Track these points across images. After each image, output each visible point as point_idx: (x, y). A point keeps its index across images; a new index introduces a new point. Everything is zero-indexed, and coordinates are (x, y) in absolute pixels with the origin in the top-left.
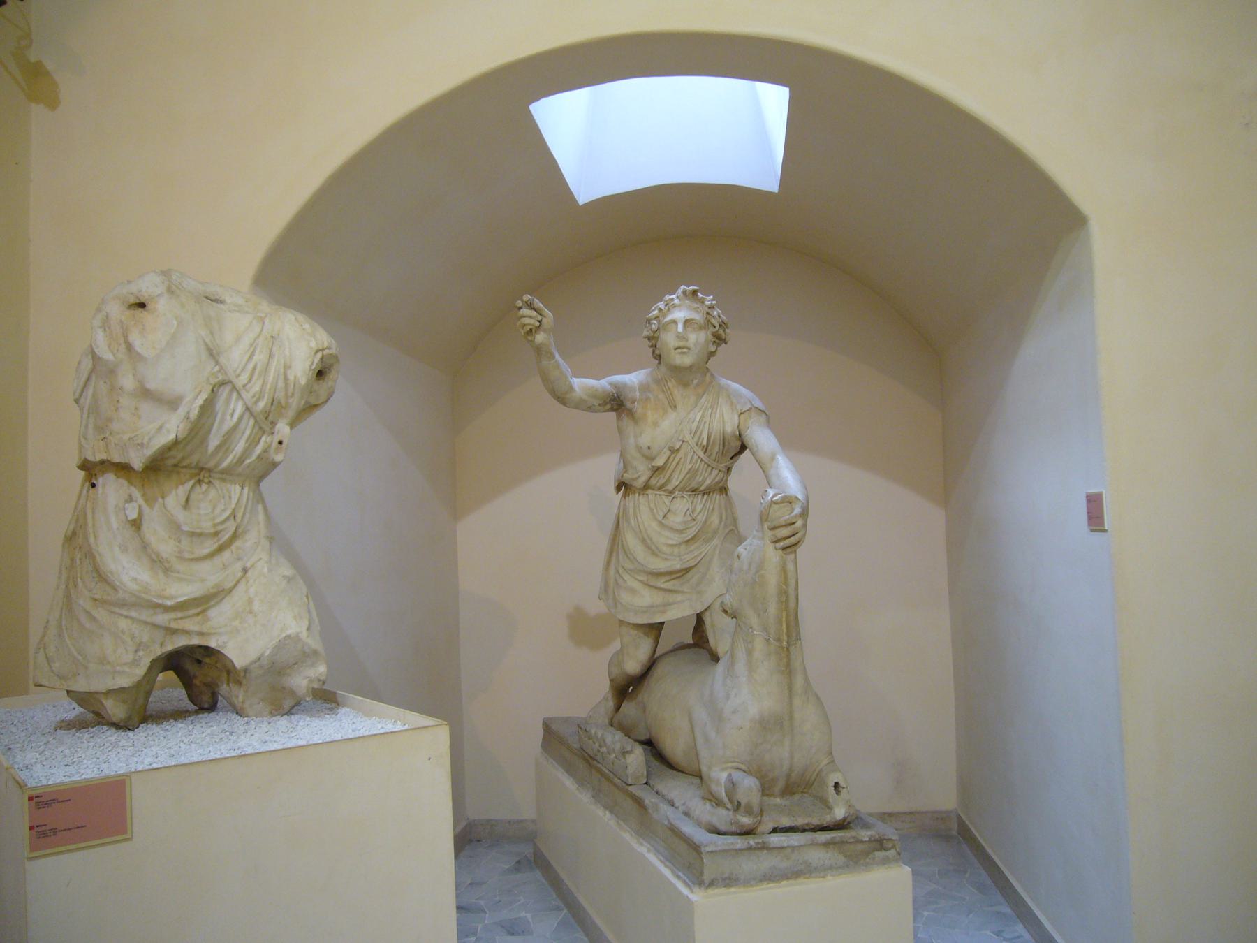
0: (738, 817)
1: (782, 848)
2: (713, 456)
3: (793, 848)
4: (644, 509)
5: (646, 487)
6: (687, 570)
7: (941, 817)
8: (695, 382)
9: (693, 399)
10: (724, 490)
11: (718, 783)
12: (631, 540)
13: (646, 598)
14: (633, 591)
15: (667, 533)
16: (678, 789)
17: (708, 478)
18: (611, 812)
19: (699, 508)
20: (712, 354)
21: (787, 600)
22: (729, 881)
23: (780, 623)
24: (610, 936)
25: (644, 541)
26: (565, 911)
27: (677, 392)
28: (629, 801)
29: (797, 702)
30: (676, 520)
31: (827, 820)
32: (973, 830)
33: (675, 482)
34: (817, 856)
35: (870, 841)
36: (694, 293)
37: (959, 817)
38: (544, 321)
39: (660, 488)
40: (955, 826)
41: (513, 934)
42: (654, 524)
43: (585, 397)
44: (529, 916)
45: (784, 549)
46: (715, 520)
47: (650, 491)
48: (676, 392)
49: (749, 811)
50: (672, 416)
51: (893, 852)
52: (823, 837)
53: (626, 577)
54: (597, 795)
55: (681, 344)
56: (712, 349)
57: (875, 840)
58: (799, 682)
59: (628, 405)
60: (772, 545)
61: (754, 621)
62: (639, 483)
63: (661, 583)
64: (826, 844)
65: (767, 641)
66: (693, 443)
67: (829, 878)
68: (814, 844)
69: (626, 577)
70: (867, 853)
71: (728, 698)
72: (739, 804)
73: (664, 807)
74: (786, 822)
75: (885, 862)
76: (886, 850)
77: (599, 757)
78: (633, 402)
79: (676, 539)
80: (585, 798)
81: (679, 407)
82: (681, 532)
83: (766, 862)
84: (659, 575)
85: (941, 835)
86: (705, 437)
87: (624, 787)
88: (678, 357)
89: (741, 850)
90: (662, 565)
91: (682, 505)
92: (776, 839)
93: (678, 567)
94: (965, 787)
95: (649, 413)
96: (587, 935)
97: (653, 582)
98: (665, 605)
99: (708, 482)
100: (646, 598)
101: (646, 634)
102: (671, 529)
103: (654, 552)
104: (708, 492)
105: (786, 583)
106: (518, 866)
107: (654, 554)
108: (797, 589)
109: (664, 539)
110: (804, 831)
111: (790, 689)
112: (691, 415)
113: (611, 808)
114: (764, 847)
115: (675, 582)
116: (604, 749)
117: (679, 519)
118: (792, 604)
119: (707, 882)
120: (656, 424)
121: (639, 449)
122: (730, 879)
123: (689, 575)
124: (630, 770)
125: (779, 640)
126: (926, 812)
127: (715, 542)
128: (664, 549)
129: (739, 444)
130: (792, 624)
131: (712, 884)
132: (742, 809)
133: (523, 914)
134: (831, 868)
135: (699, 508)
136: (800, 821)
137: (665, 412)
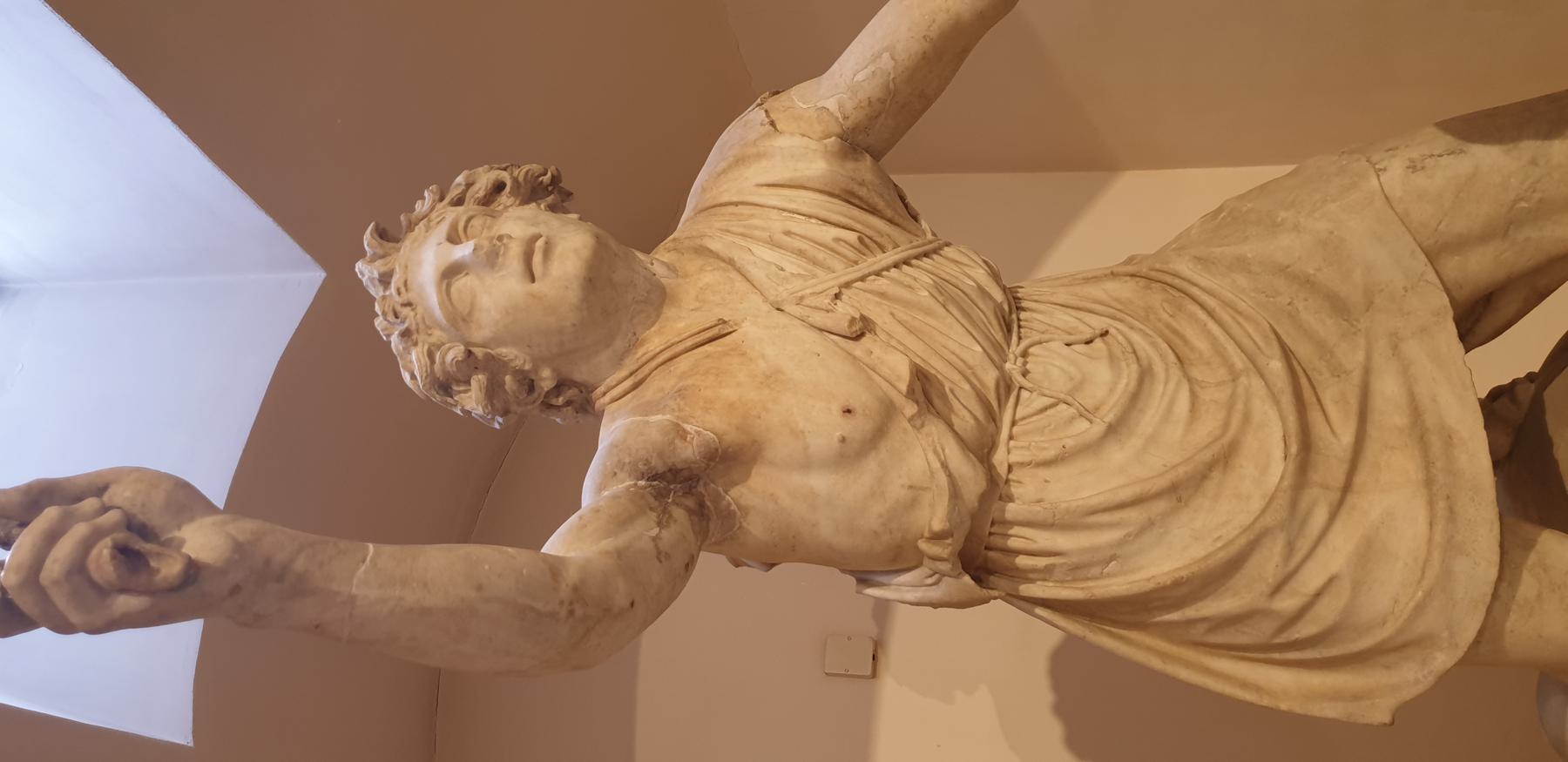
5: (982, 450)
12: (1159, 563)
13: (1393, 503)
14: (1368, 553)
15: (1147, 421)
27: (680, 322)
33: (974, 352)
42: (1117, 455)
43: (608, 544)
47: (1000, 458)
59: (688, 452)
63: (1337, 435)
69: (1311, 579)
78: (683, 434)
79: (1168, 392)
82: (1145, 374)
90: (1266, 460)
91: (1050, 365)
95: (728, 393)
97: (1330, 469)
100: (1393, 503)
101: (1528, 545)
102: (1136, 398)
107: (1224, 458)
109: (1169, 435)
110: (1495, 595)
112: (757, 273)
115: (1328, 397)
117: (1101, 373)
120: (772, 379)
121: (850, 454)
128: (1209, 425)
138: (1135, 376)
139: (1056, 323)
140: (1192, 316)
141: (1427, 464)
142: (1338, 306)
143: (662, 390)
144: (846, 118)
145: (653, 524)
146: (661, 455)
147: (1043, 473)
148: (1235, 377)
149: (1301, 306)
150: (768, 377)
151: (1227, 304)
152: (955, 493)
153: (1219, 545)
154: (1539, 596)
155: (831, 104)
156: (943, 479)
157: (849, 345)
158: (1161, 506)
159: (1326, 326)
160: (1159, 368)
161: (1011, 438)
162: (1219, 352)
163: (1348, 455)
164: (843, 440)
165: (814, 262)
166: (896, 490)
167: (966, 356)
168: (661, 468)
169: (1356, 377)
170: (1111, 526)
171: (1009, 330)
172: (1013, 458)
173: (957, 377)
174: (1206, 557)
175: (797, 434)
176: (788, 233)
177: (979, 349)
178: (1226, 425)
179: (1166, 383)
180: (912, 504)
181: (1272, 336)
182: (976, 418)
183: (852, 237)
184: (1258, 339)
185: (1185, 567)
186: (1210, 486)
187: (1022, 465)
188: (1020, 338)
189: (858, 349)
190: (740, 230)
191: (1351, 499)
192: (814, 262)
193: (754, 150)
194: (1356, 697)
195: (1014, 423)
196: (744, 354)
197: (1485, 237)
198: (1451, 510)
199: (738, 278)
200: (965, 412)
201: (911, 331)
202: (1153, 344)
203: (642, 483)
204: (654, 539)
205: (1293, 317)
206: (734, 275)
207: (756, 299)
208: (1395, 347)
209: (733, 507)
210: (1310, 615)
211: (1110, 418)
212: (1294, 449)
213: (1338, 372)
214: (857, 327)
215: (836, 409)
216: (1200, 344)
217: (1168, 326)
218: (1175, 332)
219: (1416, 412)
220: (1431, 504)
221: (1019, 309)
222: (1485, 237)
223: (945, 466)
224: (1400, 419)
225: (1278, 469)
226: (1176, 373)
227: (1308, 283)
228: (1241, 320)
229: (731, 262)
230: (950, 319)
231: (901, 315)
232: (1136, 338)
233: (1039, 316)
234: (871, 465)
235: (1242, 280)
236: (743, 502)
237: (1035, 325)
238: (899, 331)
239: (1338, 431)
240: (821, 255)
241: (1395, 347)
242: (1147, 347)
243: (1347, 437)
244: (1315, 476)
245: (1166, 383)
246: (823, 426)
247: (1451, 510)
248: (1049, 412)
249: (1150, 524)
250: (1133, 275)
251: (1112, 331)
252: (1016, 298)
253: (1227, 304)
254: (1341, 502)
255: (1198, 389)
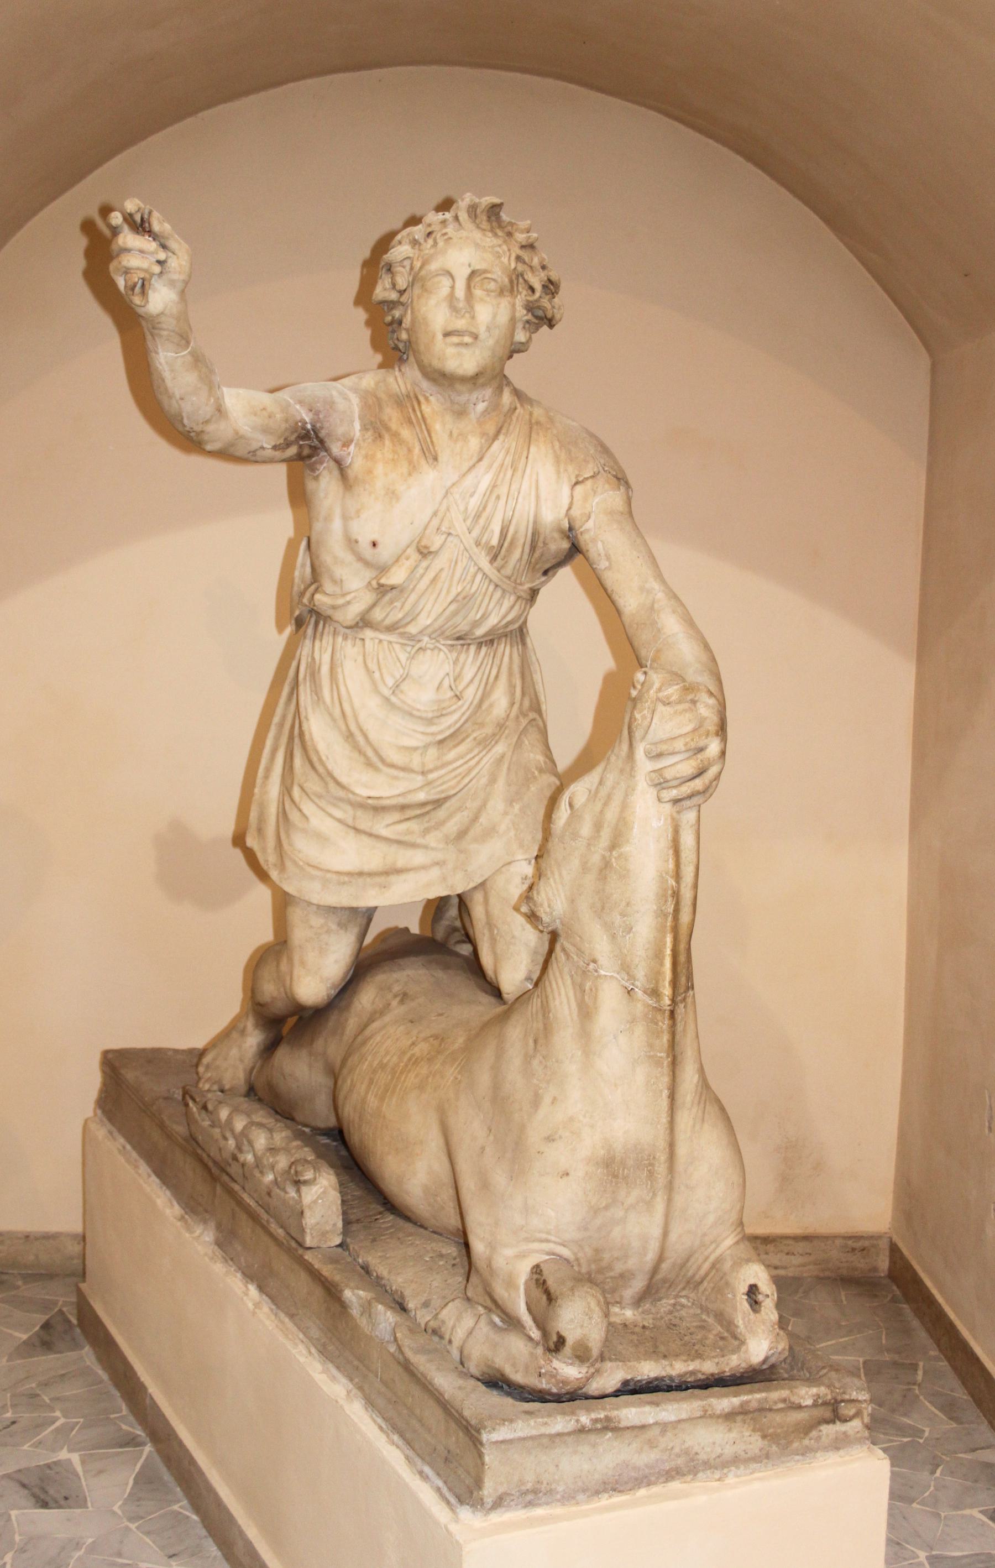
0: (556, 1364)
1: (643, 1427)
2: (508, 571)
3: (664, 1427)
4: (353, 676)
5: (364, 622)
6: (438, 803)
7: (859, 1244)
8: (481, 406)
9: (474, 443)
10: (517, 634)
11: (510, 1283)
12: (319, 729)
13: (348, 853)
14: (321, 838)
16: (407, 1266)
17: (497, 612)
18: (261, 1288)
19: (468, 674)
20: (515, 350)
21: (677, 911)
22: (534, 1495)
23: (659, 956)
24: (265, 1552)
25: (349, 736)
26: (148, 1448)
28: (303, 1276)
29: (685, 1119)
30: (422, 696)
31: (733, 1363)
32: (929, 1283)
33: (424, 620)
34: (711, 1439)
35: (815, 1405)
36: (494, 211)
37: (894, 1249)
38: (173, 263)
39: (391, 628)
40: (883, 1264)
41: (45, 1505)
42: (373, 703)
44: (75, 1458)
45: (676, 801)
46: (500, 702)
47: (368, 633)
48: (437, 427)
49: (582, 1355)
50: (429, 477)
51: (856, 1424)
52: (725, 1402)
53: (308, 808)
54: (226, 1242)
55: (460, 324)
56: (521, 336)
57: (825, 1404)
58: (689, 1077)
59: (336, 449)
60: (653, 792)
61: (601, 946)
62: (352, 613)
63: (383, 826)
64: (729, 1416)
65: (629, 992)
66: (469, 540)
67: (731, 1480)
68: (707, 1416)
70: (807, 1428)
71: (536, 1102)
72: (561, 1341)
73: (386, 1318)
74: (648, 1370)
75: (839, 1444)
76: (845, 1420)
77: (234, 1169)
78: (346, 444)
80: (200, 1240)
81: (443, 457)
83: (610, 1455)
84: (378, 809)
85: (856, 1282)
86: (496, 528)
87: (294, 1246)
88: (451, 351)
89: (559, 1435)
90: (366, 784)
92: (633, 1412)
93: (421, 796)
94: (910, 1197)
95: (379, 469)
96: (197, 1509)
97: (365, 821)
98: (386, 873)
99: (493, 621)
100: (348, 853)
101: (342, 926)
103: (372, 759)
104: (490, 640)
105: (678, 876)
106: (48, 1338)
108: (695, 886)
109: (393, 734)
111: (672, 1097)
112: (469, 480)
113: (259, 1277)
114: (609, 1426)
115: (413, 825)
116: (250, 1158)
118: (685, 918)
119: (489, 1501)
120: (392, 495)
122: (535, 1492)
123: (441, 813)
124: (310, 1220)
125: (655, 993)
126: (835, 1237)
127: (500, 749)
129: (565, 545)
130: (682, 958)
131: (499, 1503)
132: (567, 1350)
133: (63, 1455)
134: (736, 1461)
135: (468, 674)
136: (678, 1368)
137: (413, 468)
138: (424, 715)
139: (466, 668)
140: (471, 750)
141: (371, 874)
142: (462, 834)
143: (390, 419)
144: (581, 533)
145: (273, 444)
146: (329, 435)
147: (360, 659)
148: (423, 773)
149: (465, 813)
150: (393, 493)
151: (470, 770)
152: (334, 607)
153: (324, 758)
154: (311, 927)
155: (590, 524)
156: (341, 601)
157: (414, 544)
158: (344, 728)
159: (452, 827)
160: (434, 729)
161: (381, 641)
162: (443, 766)
163: (374, 831)
164: (357, 542)
165: (478, 516)
166: (339, 572)
167: (423, 615)
168: (322, 434)
169: (420, 841)
170: (332, 698)
171: (458, 638)
172: (367, 642)
173: (407, 607)
174: (317, 752)
175: (358, 512)
176: (498, 497)
177: (429, 622)
178: (392, 766)
179: (422, 733)
180: (334, 582)
181: (443, 795)
182: (383, 620)
183: (495, 542)
184: (444, 787)
185: (312, 739)
186: (356, 755)
187: (364, 645)
188: (452, 646)
189: (411, 551)
190: (506, 463)
191: (352, 833)
192: (478, 516)
193: (562, 470)
194: (260, 831)
195: (390, 642)
196: (410, 474)
197: (487, 913)
198: (344, 883)
199: (471, 463)
200: (384, 615)
201: (434, 581)
202: (449, 727)
203: (309, 426)
204: (262, 448)
205: (459, 809)
206: (475, 459)
207: (455, 478)
208: (437, 864)
209: (317, 473)
210: (293, 806)
211: (393, 699)
212: (370, 801)
213: (426, 831)
214: (425, 551)
215: (374, 537)
216: (452, 755)
217: (467, 737)
218: (463, 740)
219: (399, 871)
220: (349, 874)
221: (480, 645)
222: (487, 913)
223: (349, 603)
224: (400, 864)
225: (363, 792)
226: (429, 739)
227: (475, 819)
228: (459, 778)
229: (480, 460)
230: (446, 604)
231: (444, 575)
232: (455, 717)
233: (470, 659)
234: (349, 558)
235: (484, 781)
236: (321, 478)
237: (463, 656)
238: (431, 575)
239: (392, 827)
240: (482, 521)
241: (437, 864)
242: (449, 723)
243: (384, 832)
244: (359, 813)
245: (422, 733)
246: (365, 531)
247: (344, 883)
248: (398, 664)
249: (334, 720)
250: (508, 716)
251: (460, 703)
252: (492, 641)
253: (470, 770)
254: (348, 826)
255: (419, 751)
